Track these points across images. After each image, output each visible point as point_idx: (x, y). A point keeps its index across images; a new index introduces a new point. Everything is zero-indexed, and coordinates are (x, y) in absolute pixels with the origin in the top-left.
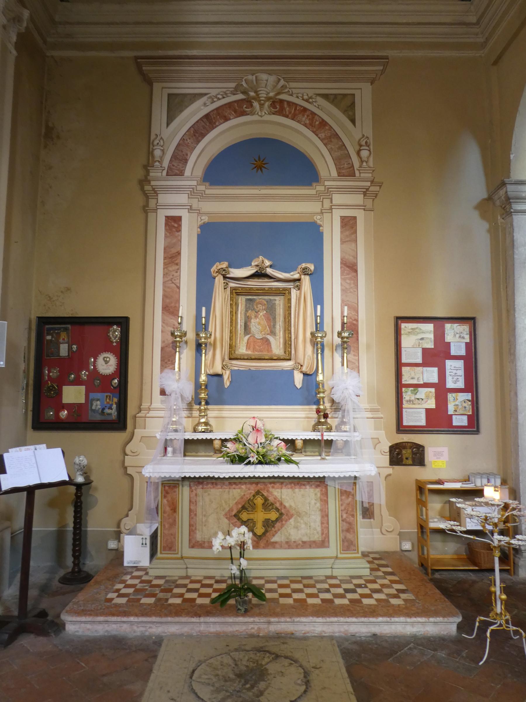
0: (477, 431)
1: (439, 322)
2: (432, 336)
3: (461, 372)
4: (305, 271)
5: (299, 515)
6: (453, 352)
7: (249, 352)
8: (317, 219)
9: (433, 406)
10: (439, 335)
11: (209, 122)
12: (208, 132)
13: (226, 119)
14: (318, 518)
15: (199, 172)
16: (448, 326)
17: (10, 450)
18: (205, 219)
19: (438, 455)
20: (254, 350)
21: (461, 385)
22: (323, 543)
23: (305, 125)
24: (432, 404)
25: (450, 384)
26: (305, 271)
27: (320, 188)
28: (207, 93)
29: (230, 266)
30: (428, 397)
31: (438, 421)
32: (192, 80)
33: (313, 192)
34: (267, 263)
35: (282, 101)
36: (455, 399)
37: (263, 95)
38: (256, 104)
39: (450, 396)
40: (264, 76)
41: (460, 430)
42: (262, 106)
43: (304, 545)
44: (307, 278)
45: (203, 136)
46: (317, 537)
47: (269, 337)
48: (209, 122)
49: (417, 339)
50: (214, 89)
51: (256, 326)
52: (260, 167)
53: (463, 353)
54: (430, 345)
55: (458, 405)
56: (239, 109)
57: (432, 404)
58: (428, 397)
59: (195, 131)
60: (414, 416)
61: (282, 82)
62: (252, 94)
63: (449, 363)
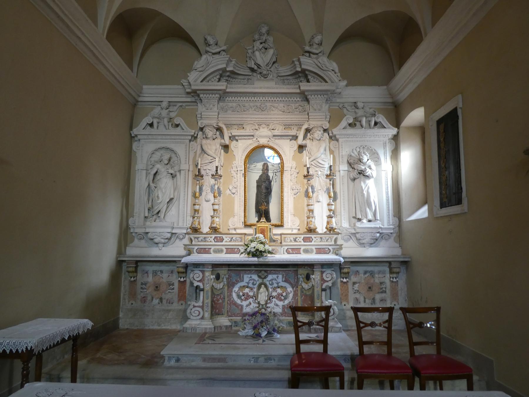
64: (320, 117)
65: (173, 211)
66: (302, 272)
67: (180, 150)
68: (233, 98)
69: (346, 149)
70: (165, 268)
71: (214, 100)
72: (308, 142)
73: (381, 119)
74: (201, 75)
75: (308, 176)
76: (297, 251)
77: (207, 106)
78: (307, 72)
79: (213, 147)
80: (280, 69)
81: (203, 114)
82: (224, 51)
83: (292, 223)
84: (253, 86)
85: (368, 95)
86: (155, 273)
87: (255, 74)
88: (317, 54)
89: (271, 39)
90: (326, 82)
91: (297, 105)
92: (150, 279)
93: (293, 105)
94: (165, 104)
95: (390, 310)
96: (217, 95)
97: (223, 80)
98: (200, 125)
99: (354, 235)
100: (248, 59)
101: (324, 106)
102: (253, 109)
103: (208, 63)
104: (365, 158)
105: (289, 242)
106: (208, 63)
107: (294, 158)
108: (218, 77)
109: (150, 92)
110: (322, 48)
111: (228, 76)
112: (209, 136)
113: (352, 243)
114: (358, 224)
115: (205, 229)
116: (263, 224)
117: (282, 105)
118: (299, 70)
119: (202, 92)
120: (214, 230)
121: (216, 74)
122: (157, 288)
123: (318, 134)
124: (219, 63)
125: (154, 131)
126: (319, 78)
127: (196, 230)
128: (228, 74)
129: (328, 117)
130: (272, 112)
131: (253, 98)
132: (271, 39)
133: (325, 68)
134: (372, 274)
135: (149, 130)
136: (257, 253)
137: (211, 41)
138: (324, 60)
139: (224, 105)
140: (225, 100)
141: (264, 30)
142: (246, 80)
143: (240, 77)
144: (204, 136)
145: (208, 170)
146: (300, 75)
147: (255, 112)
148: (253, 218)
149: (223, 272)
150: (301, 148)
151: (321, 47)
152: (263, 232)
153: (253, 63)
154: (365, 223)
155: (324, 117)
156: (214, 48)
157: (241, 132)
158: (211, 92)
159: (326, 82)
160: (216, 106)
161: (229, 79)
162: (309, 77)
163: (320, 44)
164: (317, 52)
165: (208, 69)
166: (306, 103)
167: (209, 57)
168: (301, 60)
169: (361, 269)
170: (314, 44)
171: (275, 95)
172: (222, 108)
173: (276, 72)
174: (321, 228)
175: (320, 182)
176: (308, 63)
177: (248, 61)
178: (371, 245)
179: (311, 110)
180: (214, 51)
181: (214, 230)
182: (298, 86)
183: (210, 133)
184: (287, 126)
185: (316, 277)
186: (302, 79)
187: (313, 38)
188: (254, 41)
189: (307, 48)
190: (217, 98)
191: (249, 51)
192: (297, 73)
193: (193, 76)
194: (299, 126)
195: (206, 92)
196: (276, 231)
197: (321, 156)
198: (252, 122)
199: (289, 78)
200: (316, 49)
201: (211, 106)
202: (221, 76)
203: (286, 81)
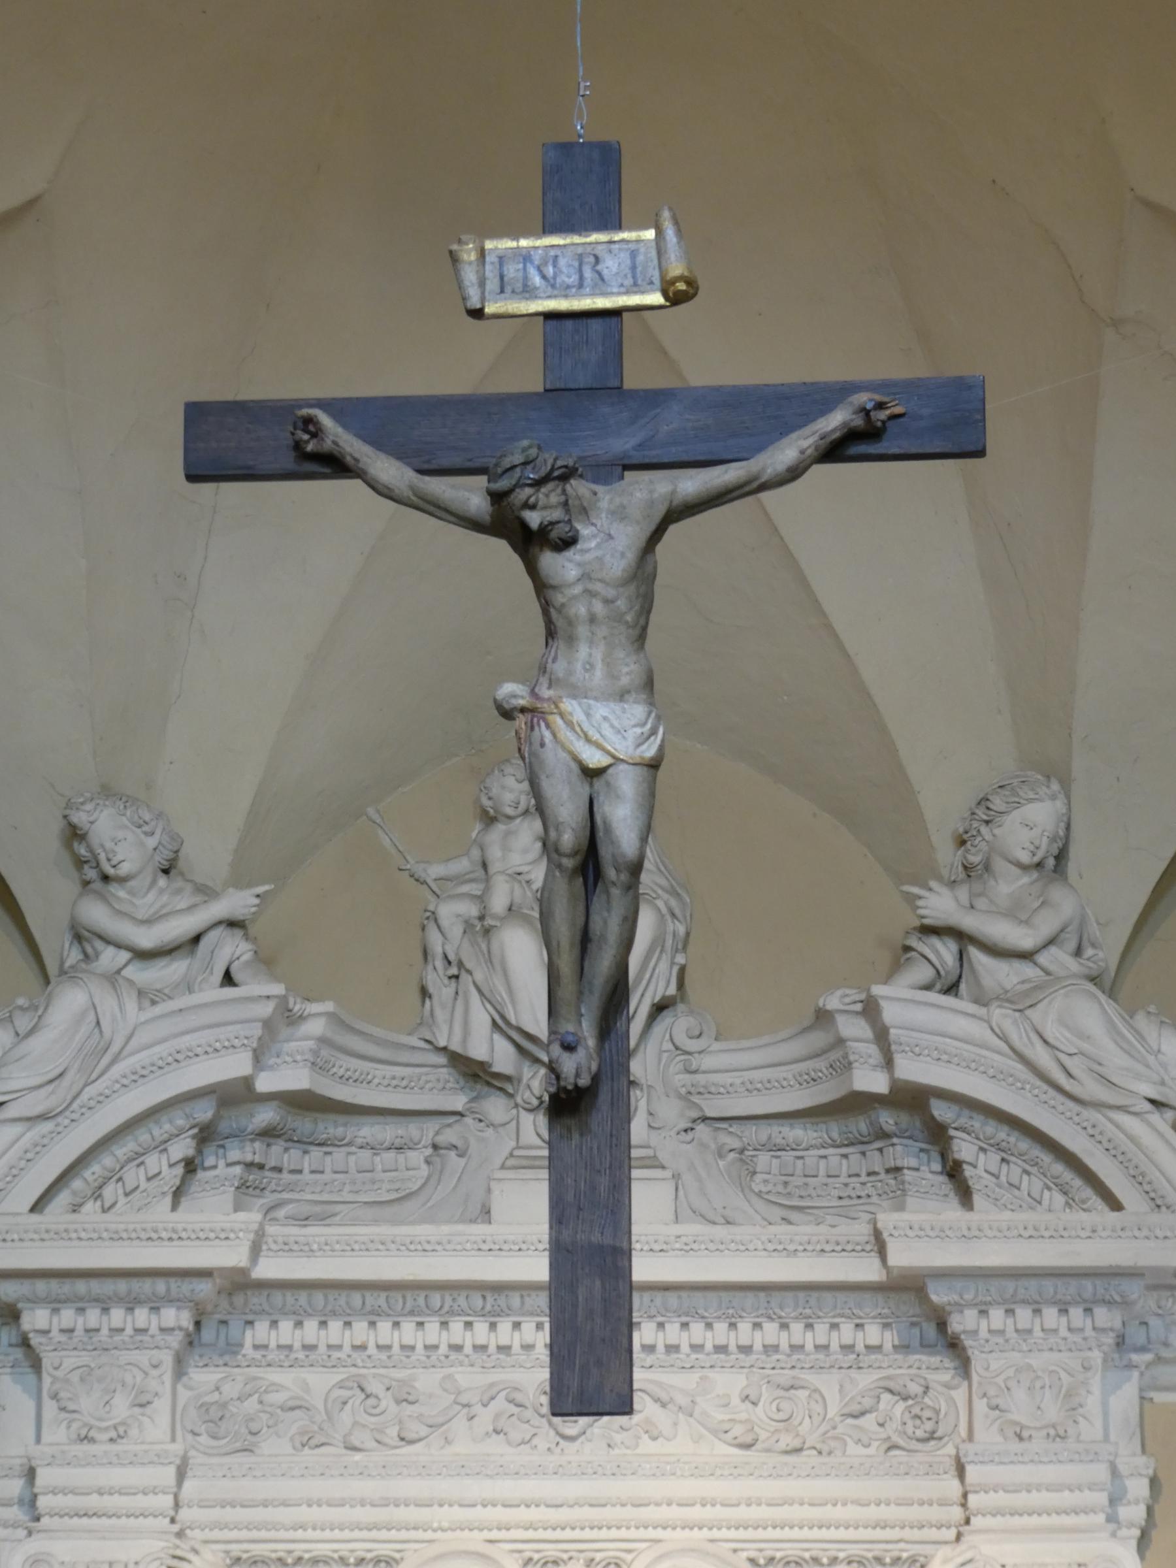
64: (1067, 1498)
68: (311, 1325)
71: (142, 1358)
74: (40, 1147)
77: (88, 1403)
78: (941, 1111)
80: (708, 1062)
81: (44, 1477)
82: (232, 924)
84: (479, 1229)
87: (496, 1107)
88: (1026, 956)
90: (1115, 1205)
91: (866, 1380)
93: (828, 1384)
96: (171, 1316)
97: (222, 1168)
100: (435, 979)
101: (1092, 1402)
102: (485, 1418)
103: (98, 1052)
106: (98, 1052)
108: (182, 1148)
110: (1064, 905)
111: (268, 1134)
112: (125, 869)
117: (730, 1382)
118: (874, 1082)
119: (41, 1286)
121: (160, 1129)
124: (195, 1038)
126: (1046, 1158)
128: (266, 1116)
129: (1139, 1488)
130: (647, 1446)
131: (481, 1327)
133: (1091, 1089)
137: (120, 839)
138: (1080, 1021)
139: (230, 1390)
140: (233, 1348)
142: (416, 1157)
143: (369, 1130)
144: (91, 874)
146: (887, 1119)
147: (496, 1446)
151: (1057, 893)
153: (481, 1017)
155: (1102, 1498)
156: (147, 903)
158: (122, 1286)
159: (1115, 1205)
160: (162, 1406)
161: (276, 1153)
162: (964, 1149)
163: (1055, 863)
164: (1024, 939)
165: (104, 1098)
166: (937, 1370)
167: (107, 1003)
168: (890, 1013)
170: (999, 864)
171: (672, 1299)
172: (214, 1416)
173: (681, 1080)
176: (941, 1042)
177: (442, 991)
179: (988, 1436)
180: (146, 939)
182: (860, 1230)
186: (903, 1153)
187: (984, 810)
188: (489, 819)
189: (941, 905)
190: (175, 1341)
191: (453, 912)
192: (856, 1103)
195: (81, 1286)
198: (475, 1540)
199: (796, 1133)
200: (1014, 912)
201: (121, 1407)
202: (206, 1135)
203: (763, 1159)
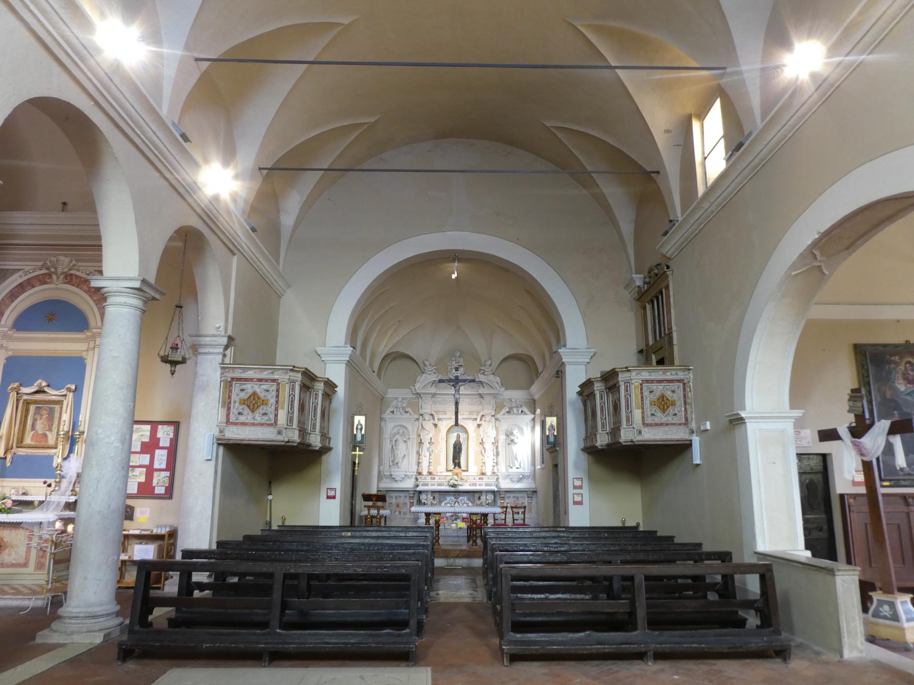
0: (171, 497)
1: (154, 425)
2: (148, 434)
3: (165, 458)
4: (69, 390)
5: (12, 547)
6: (161, 445)
7: (33, 443)
8: (84, 354)
9: (143, 480)
10: (154, 432)
11: (22, 287)
12: (20, 294)
13: (33, 287)
14: (25, 549)
15: (11, 322)
16: (160, 427)
17: (241, 539)
18: (10, 353)
19: (142, 513)
20: (36, 441)
21: (164, 466)
22: (25, 565)
23: (85, 291)
24: (142, 479)
25: (156, 465)
26: (69, 390)
27: (89, 334)
28: (24, 268)
29: (21, 385)
30: (140, 474)
31: (146, 491)
32: (15, 260)
33: (84, 336)
34: (44, 384)
35: (72, 275)
36: (159, 476)
37: (60, 271)
38: (54, 277)
39: (156, 474)
40: (62, 258)
41: (159, 497)
42: (58, 278)
43: (12, 565)
44: (71, 394)
45: (16, 297)
46: (22, 561)
47: (48, 433)
48: (22, 287)
49: (143, 433)
50: (27, 266)
51: (39, 426)
52: (50, 320)
53: (168, 445)
54: (147, 440)
55: (160, 480)
56: (42, 280)
57: (142, 479)
58: (140, 474)
59: (12, 294)
60: (133, 489)
61: (74, 262)
62: (53, 270)
63: (157, 452)
65: (406, 461)
66: (477, 495)
67: (409, 426)
69: (504, 426)
70: (402, 494)
72: (482, 422)
73: (525, 409)
75: (482, 443)
76: (475, 485)
79: (428, 425)
83: (474, 470)
85: (518, 395)
86: (396, 498)
89: (462, 360)
92: (394, 501)
94: (400, 400)
95: (506, 507)
98: (421, 412)
99: (507, 476)
104: (515, 432)
105: (471, 480)
107: (475, 431)
109: (391, 393)
113: (508, 481)
114: (510, 470)
115: (425, 473)
116: (457, 470)
120: (430, 473)
122: (398, 506)
123: (488, 418)
124: (434, 377)
125: (394, 416)
127: (420, 474)
132: (462, 360)
134: (518, 498)
135: (391, 415)
136: (454, 486)
138: (492, 377)
141: (458, 354)
145: (426, 439)
148: (451, 466)
149: (436, 495)
150: (479, 426)
152: (457, 474)
154: (514, 470)
157: (444, 416)
169: (512, 495)
174: (489, 472)
175: (489, 446)
178: (518, 482)
181: (430, 473)
183: (427, 417)
184: (471, 413)
185: (483, 498)
193: (417, 386)
194: (478, 413)
196: (464, 473)
197: (489, 431)
